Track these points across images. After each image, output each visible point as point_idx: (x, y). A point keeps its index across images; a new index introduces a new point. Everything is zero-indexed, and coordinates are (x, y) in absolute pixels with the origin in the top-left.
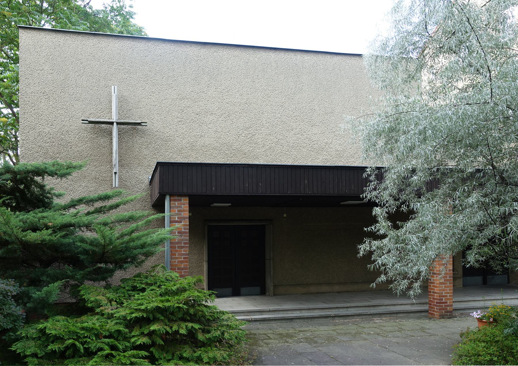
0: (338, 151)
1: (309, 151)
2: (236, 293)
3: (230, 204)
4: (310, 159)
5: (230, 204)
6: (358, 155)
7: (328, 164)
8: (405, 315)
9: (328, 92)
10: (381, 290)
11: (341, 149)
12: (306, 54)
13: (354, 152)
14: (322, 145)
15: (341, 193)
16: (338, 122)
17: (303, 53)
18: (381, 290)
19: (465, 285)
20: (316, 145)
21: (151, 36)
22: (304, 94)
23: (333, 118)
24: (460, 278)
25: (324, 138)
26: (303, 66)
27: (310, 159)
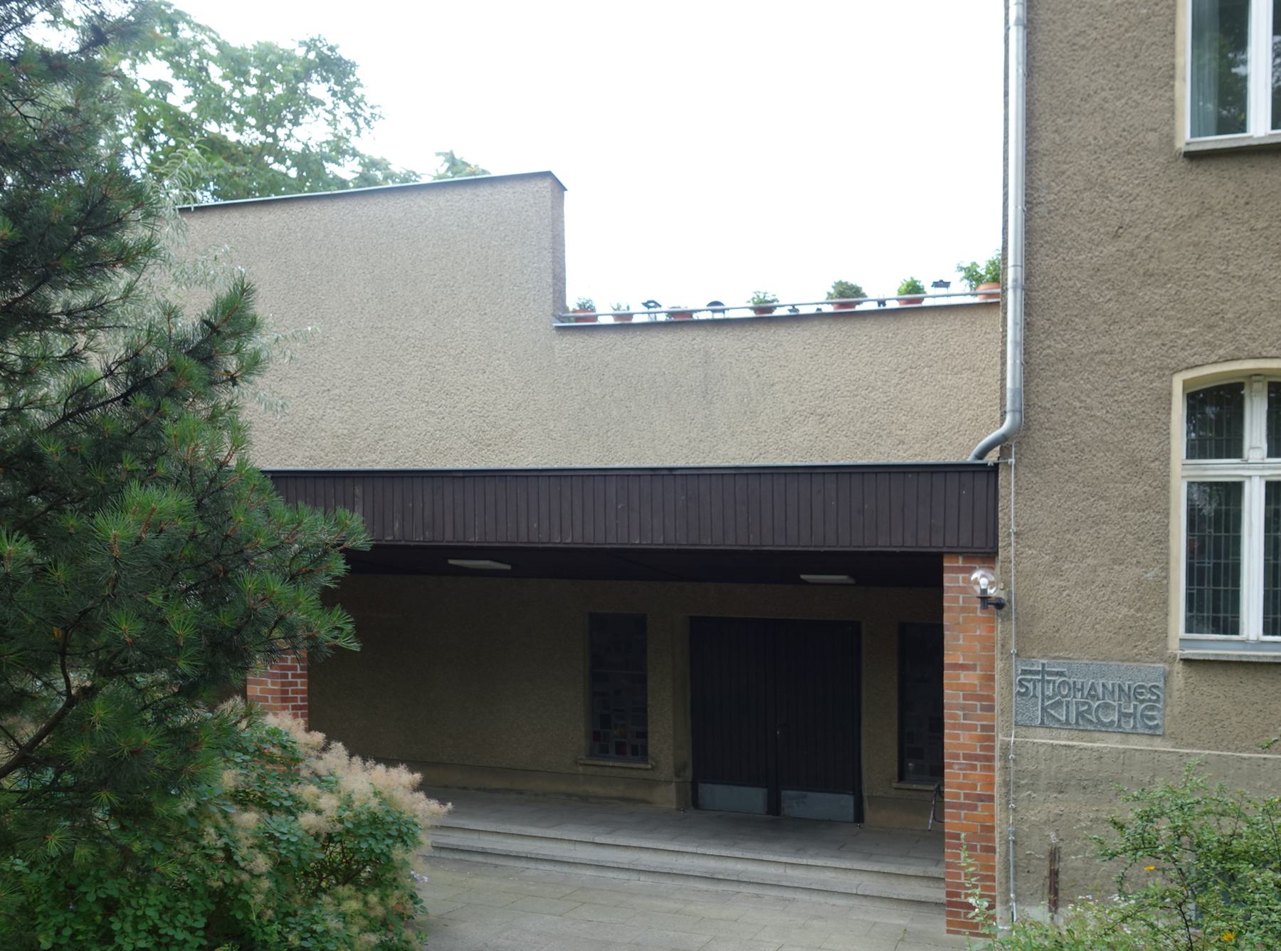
0: (338, 437)
1: (276, 439)
2: (792, 789)
3: (508, 567)
4: (278, 459)
5: (508, 567)
6: (385, 445)
7: (317, 468)
8: (604, 864)
9: (315, 293)
10: (446, 786)
11: (345, 432)
12: (265, 208)
13: (376, 439)
14: (301, 423)
15: (592, 542)
16: (338, 366)
17: (259, 208)
18: (446, 786)
19: (695, 802)
20: (290, 425)
21: (495, 172)
22: (263, 306)
23: (327, 357)
24: (668, 782)
25: (306, 407)
26: (259, 239)
27: (278, 459)
